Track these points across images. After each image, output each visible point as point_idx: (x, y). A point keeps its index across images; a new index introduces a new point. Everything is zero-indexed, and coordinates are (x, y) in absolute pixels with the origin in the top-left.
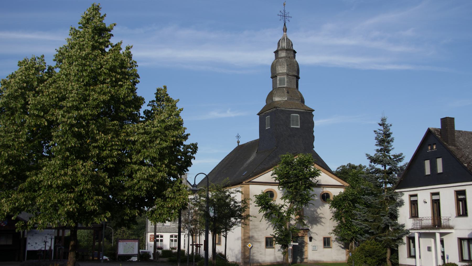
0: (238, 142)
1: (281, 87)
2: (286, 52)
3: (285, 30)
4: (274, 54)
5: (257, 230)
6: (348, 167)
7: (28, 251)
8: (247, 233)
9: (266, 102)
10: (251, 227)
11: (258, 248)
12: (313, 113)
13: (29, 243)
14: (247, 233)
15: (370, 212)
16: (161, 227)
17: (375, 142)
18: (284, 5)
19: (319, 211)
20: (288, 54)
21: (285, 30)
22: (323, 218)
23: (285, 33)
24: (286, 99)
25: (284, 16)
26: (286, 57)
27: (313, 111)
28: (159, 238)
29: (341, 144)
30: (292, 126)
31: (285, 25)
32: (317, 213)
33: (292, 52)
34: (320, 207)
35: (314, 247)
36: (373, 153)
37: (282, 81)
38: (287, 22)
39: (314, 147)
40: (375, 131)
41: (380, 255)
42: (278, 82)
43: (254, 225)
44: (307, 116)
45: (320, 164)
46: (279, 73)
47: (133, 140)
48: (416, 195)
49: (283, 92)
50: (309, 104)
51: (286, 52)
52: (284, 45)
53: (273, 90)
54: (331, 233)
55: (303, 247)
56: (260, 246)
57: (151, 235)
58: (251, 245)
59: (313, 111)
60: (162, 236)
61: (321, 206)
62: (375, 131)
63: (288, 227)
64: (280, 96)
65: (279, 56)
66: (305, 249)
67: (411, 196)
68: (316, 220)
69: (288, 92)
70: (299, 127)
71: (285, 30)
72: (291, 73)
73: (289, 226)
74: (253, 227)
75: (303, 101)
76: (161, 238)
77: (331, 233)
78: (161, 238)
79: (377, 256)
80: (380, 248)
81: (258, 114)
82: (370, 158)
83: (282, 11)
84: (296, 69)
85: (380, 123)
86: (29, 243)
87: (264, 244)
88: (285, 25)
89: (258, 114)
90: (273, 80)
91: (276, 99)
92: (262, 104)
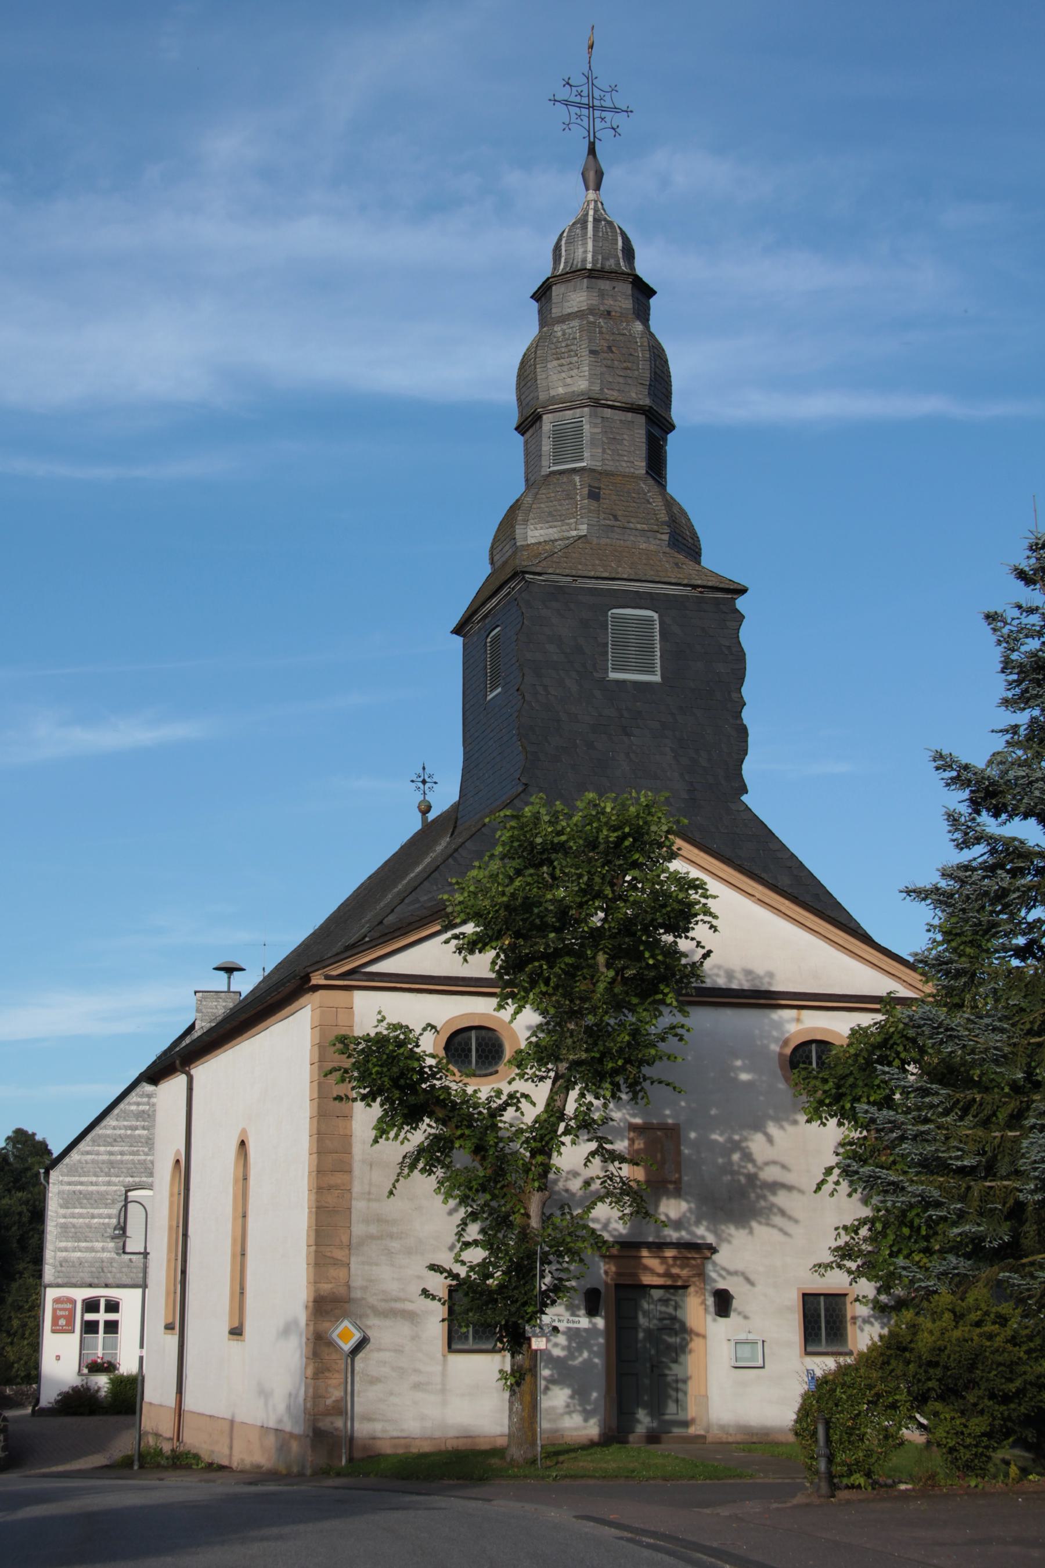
0: (425, 809)
1: (561, 472)
2: (603, 291)
3: (594, 177)
4: (535, 306)
5: (395, 1245)
8: (336, 1263)
9: (492, 562)
10: (358, 1229)
11: (399, 1350)
12: (741, 603)
14: (336, 1263)
15: (965, 1111)
16: (111, 1261)
17: (999, 686)
18: (591, 47)
19: (757, 1145)
20: (602, 294)
21: (594, 177)
22: (789, 1188)
23: (591, 195)
24: (583, 529)
25: (589, 103)
26: (591, 311)
27: (743, 591)
28: (102, 1317)
30: (613, 675)
31: (592, 151)
32: (748, 1157)
33: (627, 288)
34: (772, 1129)
35: (745, 1351)
36: (980, 747)
37: (567, 441)
38: (605, 135)
39: (744, 790)
40: (991, 618)
41: (1012, 1387)
42: (547, 446)
43: (380, 1220)
44: (707, 624)
45: (784, 881)
46: (553, 400)
49: (570, 497)
50: (718, 559)
51: (603, 291)
52: (586, 253)
54: (828, 1266)
55: (680, 1350)
56: (415, 1338)
57: (57, 1301)
58: (357, 1336)
59: (743, 591)
60: (113, 1306)
61: (777, 1120)
62: (991, 618)
63: (535, 1223)
64: (552, 517)
65: (556, 312)
66: (691, 1363)
68: (742, 1199)
69: (594, 495)
70: (657, 678)
71: (591, 175)
72: (612, 395)
73: (546, 1219)
74: (373, 1229)
76: (111, 1317)
77: (828, 1266)
78: (111, 1317)
79: (992, 1396)
80: (1013, 1340)
81: (457, 631)
82: (961, 776)
83: (578, 80)
84: (644, 370)
85: (1024, 565)
88: (592, 151)
89: (457, 631)
90: (526, 443)
91: (534, 533)
92: (478, 572)
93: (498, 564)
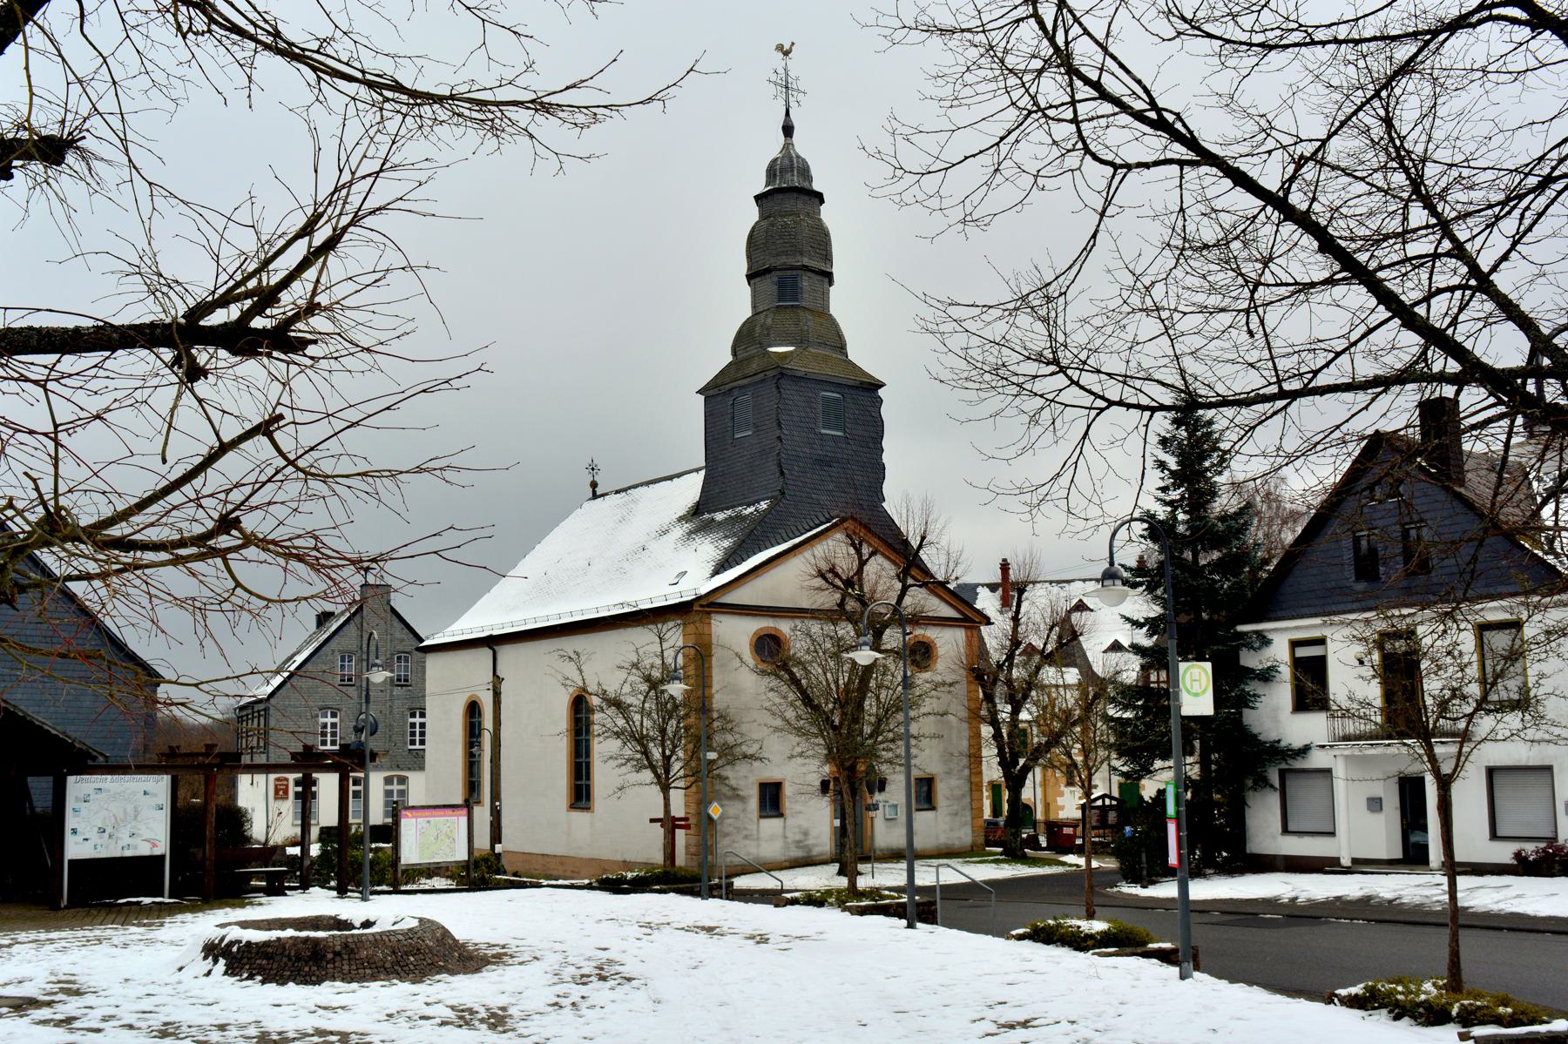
6: (1159, 592)
7: (70, 861)
9: (734, 353)
11: (737, 818)
12: (881, 392)
13: (74, 831)
27: (882, 385)
29: (1025, 508)
47: (1141, 605)
48: (1321, 641)
53: (756, 314)
56: (744, 810)
59: (882, 385)
67: (1295, 644)
75: (841, 347)
83: (781, 71)
86: (74, 831)
87: (753, 803)
93: (741, 355)
